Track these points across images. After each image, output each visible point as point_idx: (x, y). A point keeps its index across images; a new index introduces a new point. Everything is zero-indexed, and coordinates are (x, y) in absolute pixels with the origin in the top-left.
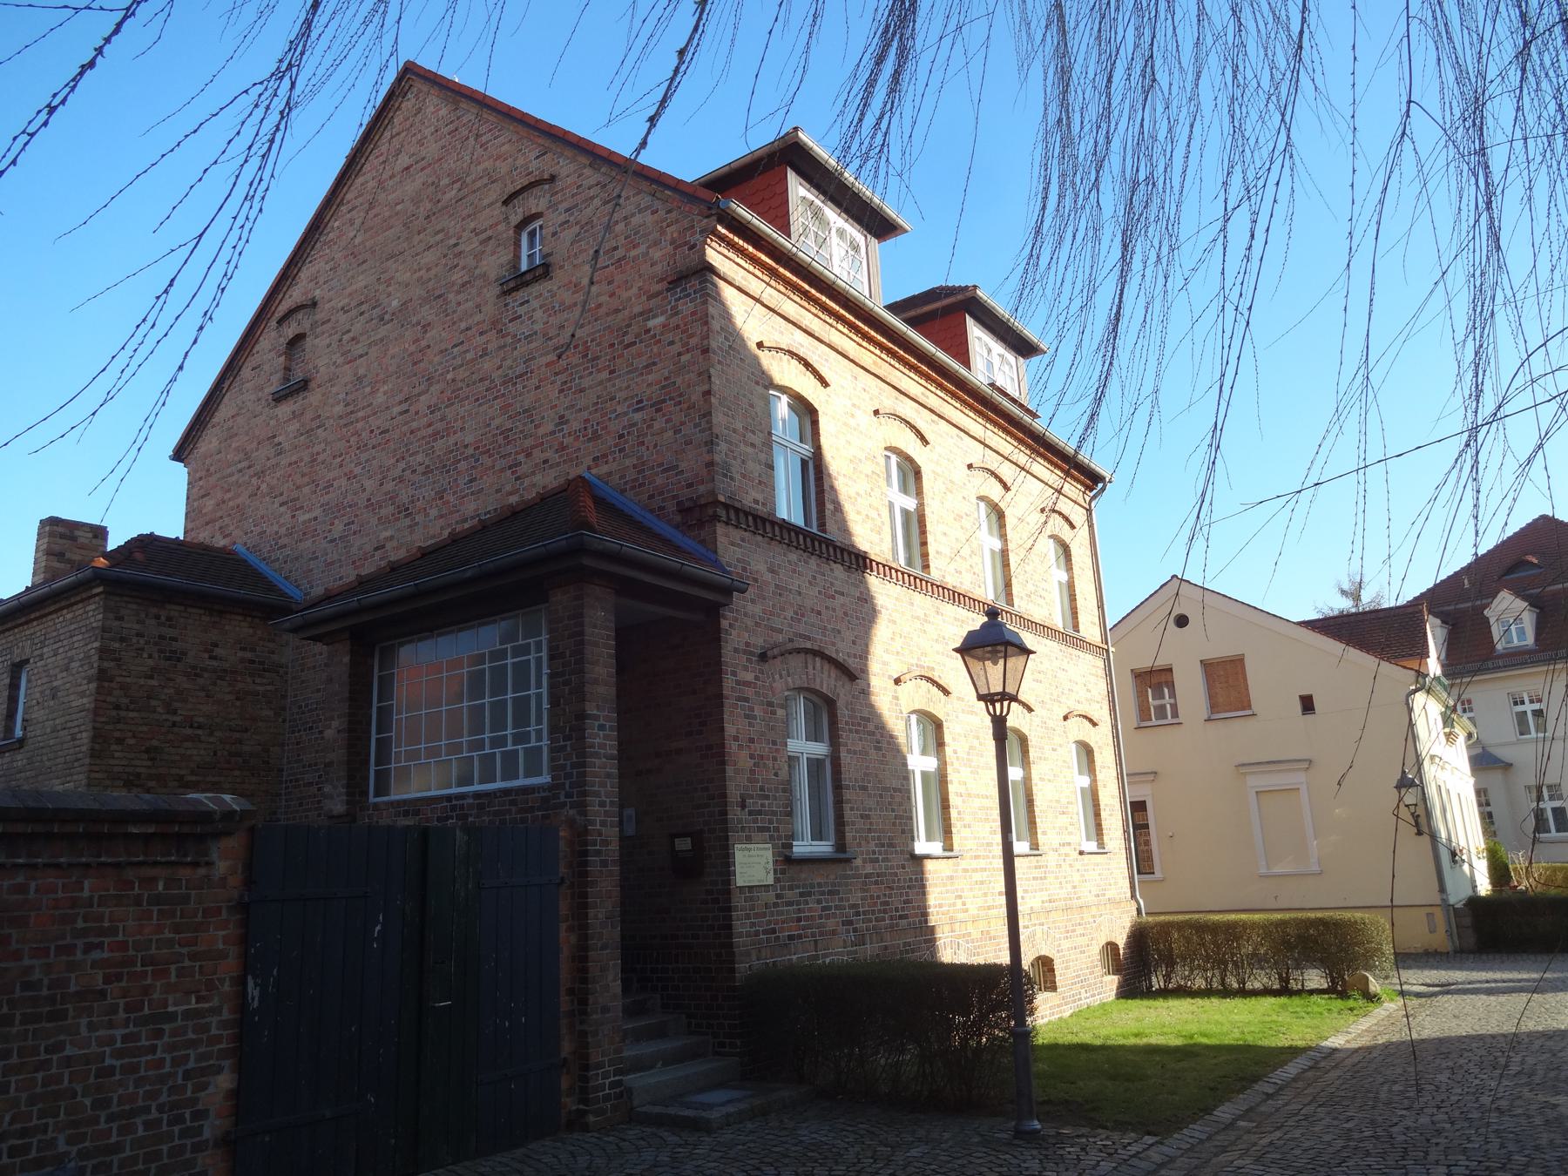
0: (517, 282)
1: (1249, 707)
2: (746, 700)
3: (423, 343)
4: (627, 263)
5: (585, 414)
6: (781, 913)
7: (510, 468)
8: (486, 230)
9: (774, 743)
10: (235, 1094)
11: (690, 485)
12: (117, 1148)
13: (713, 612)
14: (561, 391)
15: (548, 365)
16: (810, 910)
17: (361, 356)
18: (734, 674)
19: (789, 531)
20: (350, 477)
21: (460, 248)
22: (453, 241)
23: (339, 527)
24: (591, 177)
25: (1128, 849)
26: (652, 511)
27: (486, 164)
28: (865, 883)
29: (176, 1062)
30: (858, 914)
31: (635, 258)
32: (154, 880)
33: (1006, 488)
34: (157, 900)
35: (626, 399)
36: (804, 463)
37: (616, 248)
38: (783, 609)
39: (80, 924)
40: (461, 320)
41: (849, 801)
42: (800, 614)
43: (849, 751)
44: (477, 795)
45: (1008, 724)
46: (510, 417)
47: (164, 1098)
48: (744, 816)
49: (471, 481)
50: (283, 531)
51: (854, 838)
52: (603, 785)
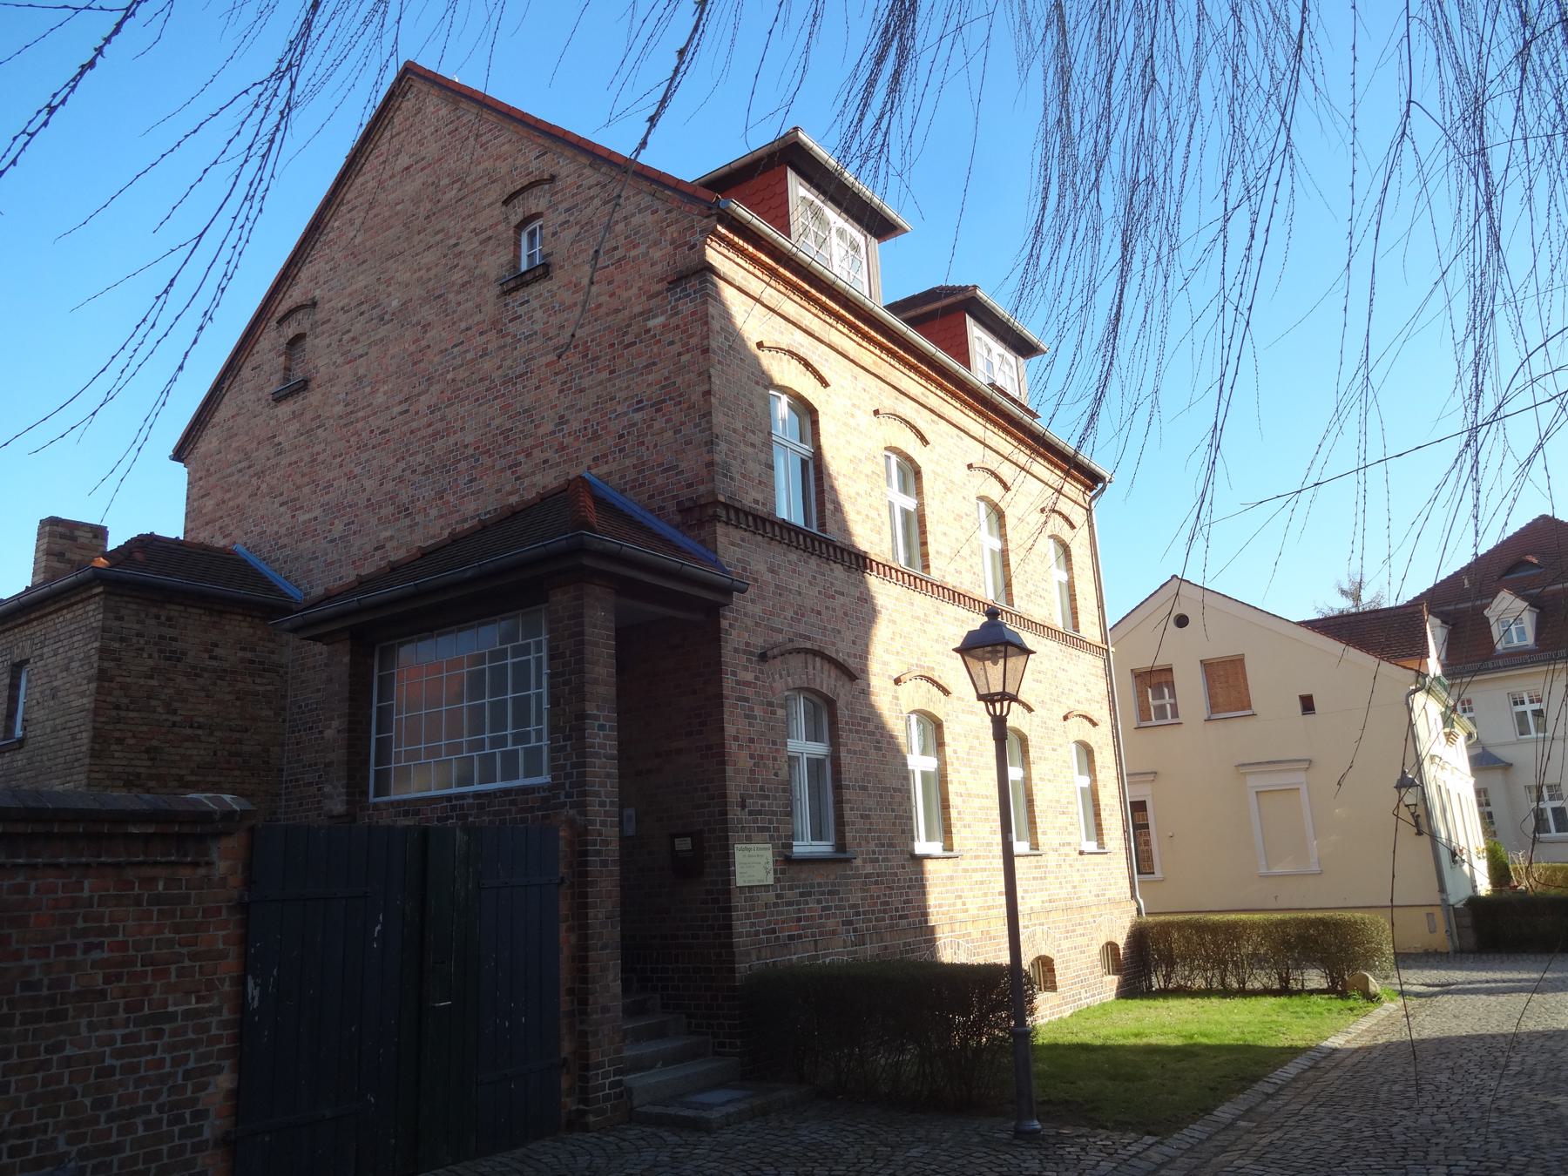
0: (517, 282)
1: (1249, 707)
2: (746, 700)
3: (423, 343)
4: (627, 263)
5: (585, 414)
6: (781, 913)
8: (486, 230)
9: (774, 743)
10: (235, 1094)
11: (690, 485)
12: (117, 1148)
13: (713, 612)
14: (561, 391)
15: (548, 365)
16: (810, 910)
17: (361, 356)
18: (734, 674)
19: (789, 531)
20: (350, 477)
21: (460, 248)
22: (453, 241)
23: (339, 527)
24: (591, 177)
25: (1128, 849)
26: (652, 511)
27: (486, 164)
28: (865, 883)
29: (176, 1062)
30: (858, 914)
31: (635, 258)
32: (154, 880)
33: (1006, 488)
34: (157, 900)
35: (626, 399)
36: (804, 463)
37: (616, 248)
38: (783, 609)
39: (80, 924)
40: (461, 320)
41: (849, 801)
42: (800, 614)
43: (849, 751)
45: (1008, 724)
46: (510, 417)
47: (164, 1098)
48: (744, 816)
49: (471, 481)
50: (283, 531)
51: (854, 838)
52: (603, 785)
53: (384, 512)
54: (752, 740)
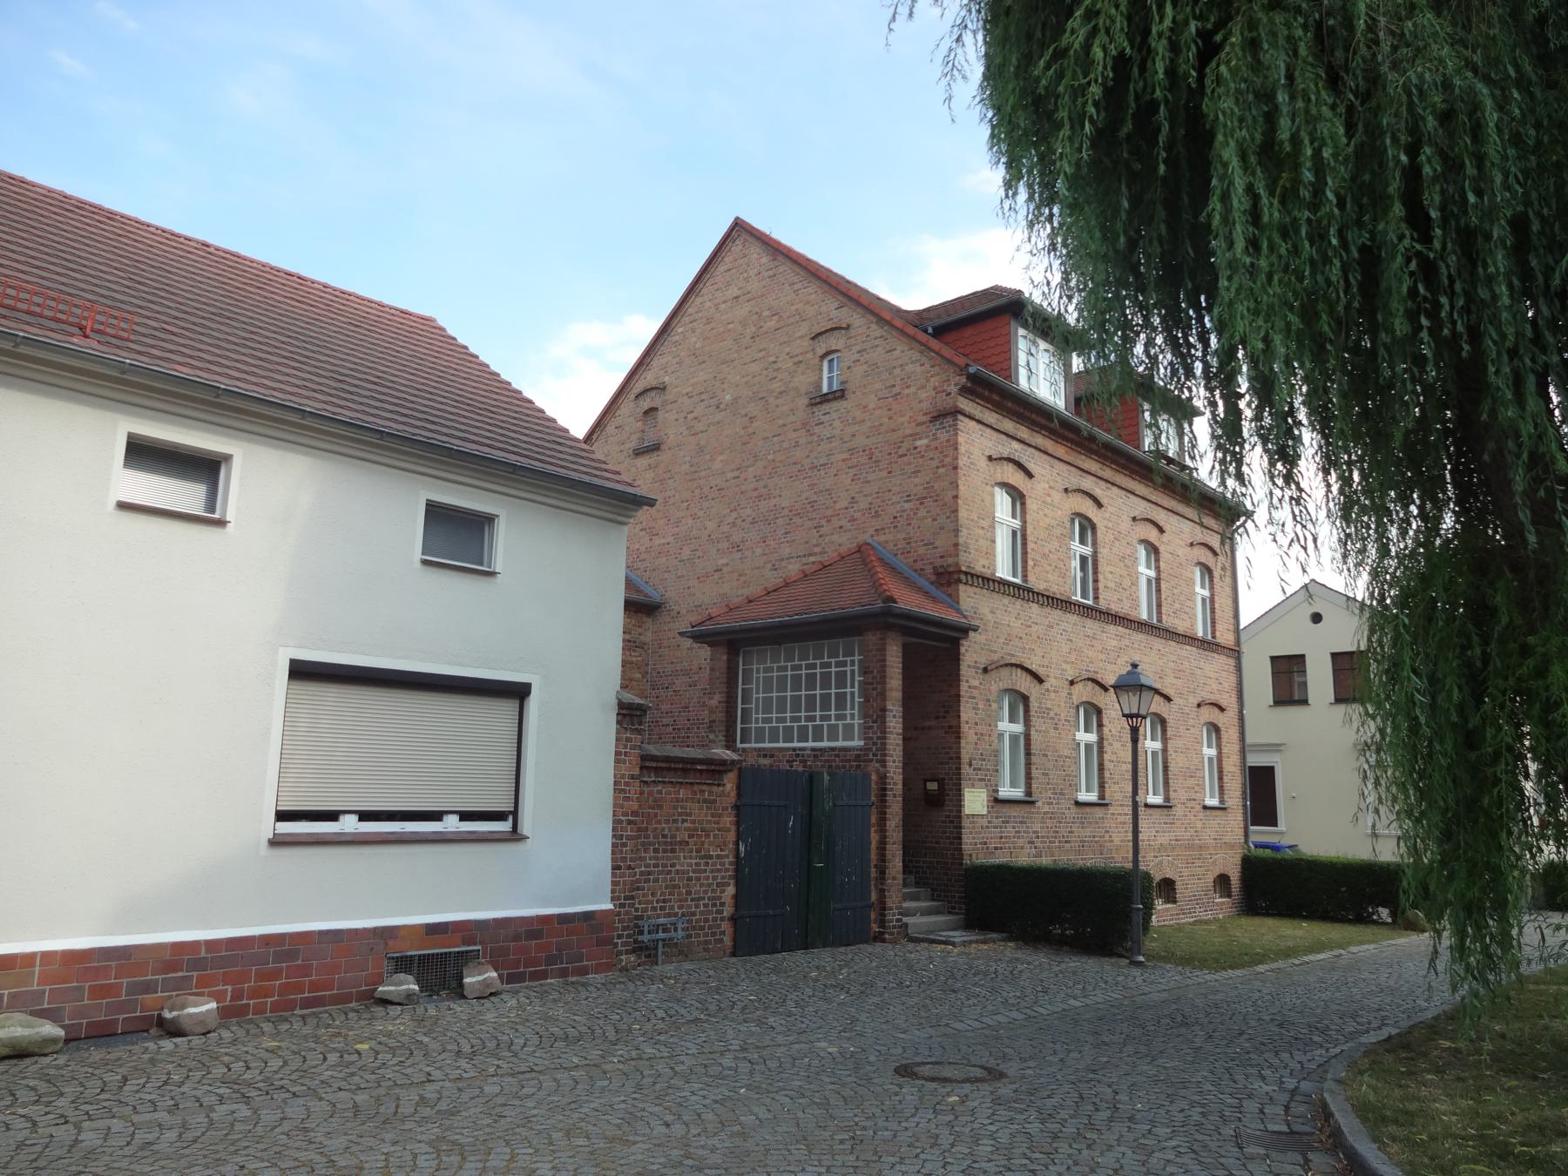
0: (821, 399)
2: (974, 698)
3: (750, 430)
4: (902, 398)
5: (870, 499)
6: (991, 833)
7: (815, 528)
8: (797, 356)
9: (990, 725)
10: (736, 897)
11: (942, 557)
12: (694, 914)
13: (955, 644)
14: (852, 480)
15: (843, 460)
16: (1008, 832)
17: (702, 432)
18: (967, 681)
19: (1004, 585)
20: (694, 517)
21: (779, 365)
22: (772, 359)
23: (686, 552)
24: (876, 331)
25: (1245, 806)
26: (916, 571)
27: (798, 306)
28: (1043, 818)
29: (715, 878)
30: (1038, 837)
31: (908, 395)
32: (704, 791)
33: (1161, 530)
34: (705, 801)
35: (899, 493)
36: (1014, 533)
37: (894, 386)
38: (998, 637)
39: (680, 810)
40: (779, 418)
41: (1035, 764)
42: (1009, 639)
43: (1037, 731)
44: (813, 749)
46: (815, 493)
47: (709, 894)
48: (971, 771)
49: (786, 533)
50: (643, 549)
51: (1038, 788)
52: (895, 750)
53: (720, 546)
54: (976, 724)
